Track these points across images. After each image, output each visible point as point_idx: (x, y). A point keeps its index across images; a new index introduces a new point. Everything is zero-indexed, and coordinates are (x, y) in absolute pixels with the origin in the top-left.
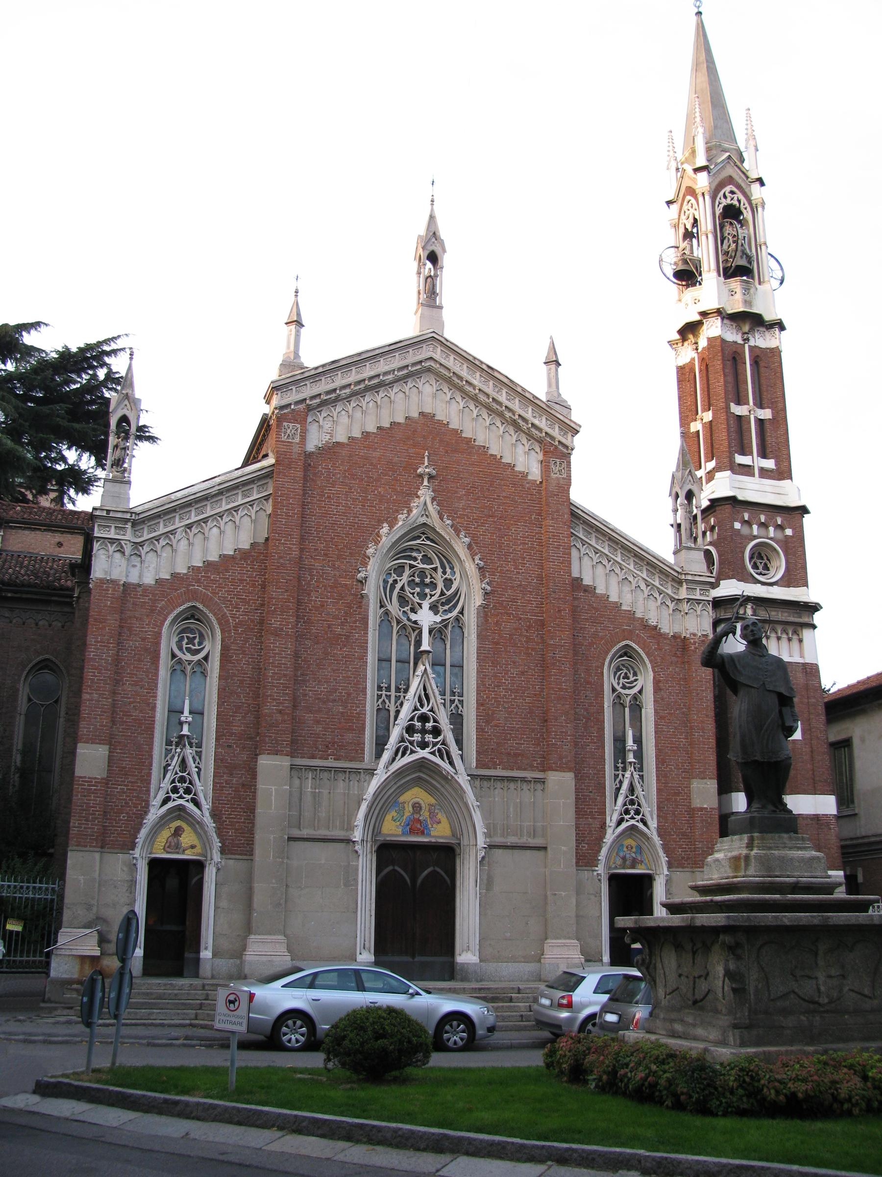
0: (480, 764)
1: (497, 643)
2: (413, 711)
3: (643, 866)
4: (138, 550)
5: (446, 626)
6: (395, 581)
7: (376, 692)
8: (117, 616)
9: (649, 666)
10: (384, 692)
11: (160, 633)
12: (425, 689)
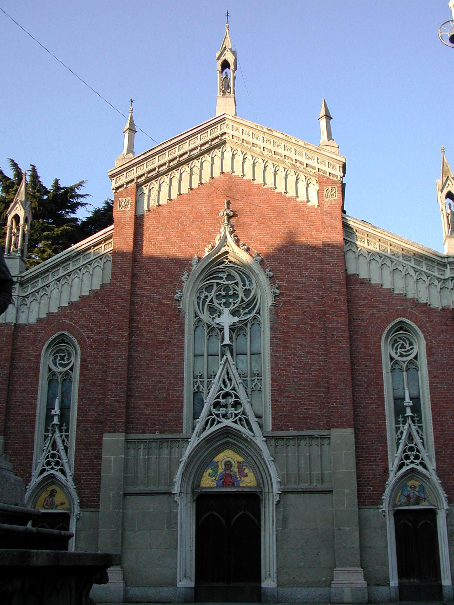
0: (275, 427)
1: (287, 333)
2: (219, 391)
3: (426, 503)
4: (26, 301)
5: (246, 325)
6: (206, 297)
7: (262, 378)
8: (10, 347)
9: (422, 335)
10: (199, 379)
11: (40, 355)
12: (228, 374)
